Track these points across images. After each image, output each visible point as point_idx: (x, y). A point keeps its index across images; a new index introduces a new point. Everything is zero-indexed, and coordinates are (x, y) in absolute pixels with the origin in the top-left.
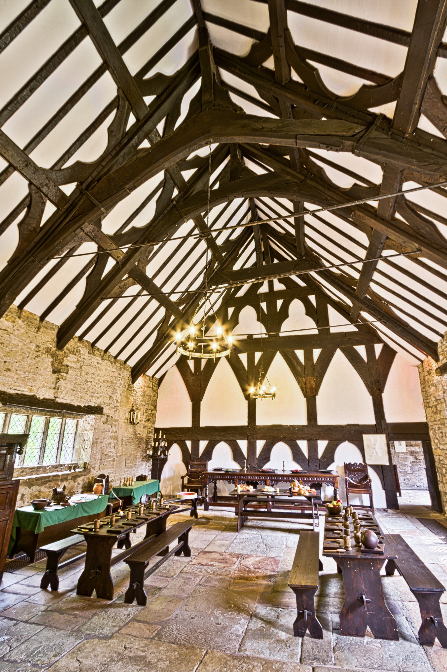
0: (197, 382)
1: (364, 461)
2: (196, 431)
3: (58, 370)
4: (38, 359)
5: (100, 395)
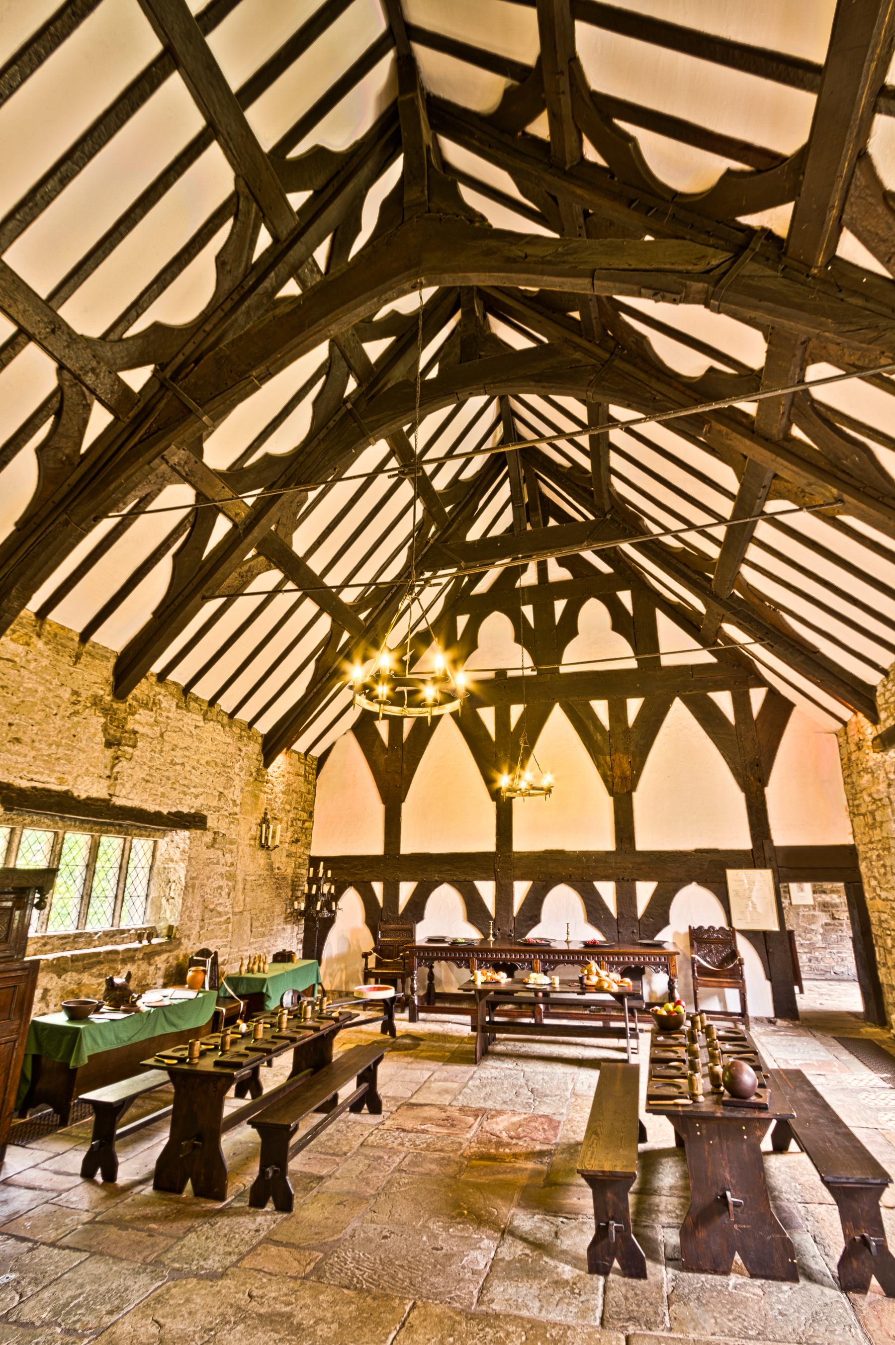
1: (730, 923)
2: (392, 863)
3: (116, 741)
4: (75, 719)
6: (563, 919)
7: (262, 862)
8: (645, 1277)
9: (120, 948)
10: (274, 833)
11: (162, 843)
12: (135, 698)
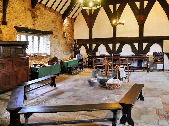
1: (163, 51)
2: (91, 40)
3: (34, 17)
4: (26, 13)
5: (51, 26)
6: (102, 50)
7: (64, 41)
9: (41, 56)
10: (66, 35)
11: (45, 37)
12: (36, 8)
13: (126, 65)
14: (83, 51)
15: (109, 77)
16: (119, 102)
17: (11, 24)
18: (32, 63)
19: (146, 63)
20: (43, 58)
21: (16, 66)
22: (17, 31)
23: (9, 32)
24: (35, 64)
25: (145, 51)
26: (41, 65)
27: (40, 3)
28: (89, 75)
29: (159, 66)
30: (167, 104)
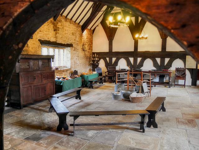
0: (111, 33)
1: (185, 67)
2: (111, 54)
3: (56, 29)
4: (49, 26)
5: (71, 39)
6: (122, 64)
8: (165, 111)
11: (65, 50)
13: (149, 80)
14: (102, 64)
15: (132, 91)
16: (147, 108)
17: (36, 37)
18: (57, 77)
19: (167, 78)
20: (63, 71)
21: (44, 79)
22: (41, 45)
23: (35, 45)
24: (58, 77)
25: (168, 66)
26: (64, 78)
27: (61, 15)
28: (111, 89)
29: (181, 82)
30: (186, 114)
